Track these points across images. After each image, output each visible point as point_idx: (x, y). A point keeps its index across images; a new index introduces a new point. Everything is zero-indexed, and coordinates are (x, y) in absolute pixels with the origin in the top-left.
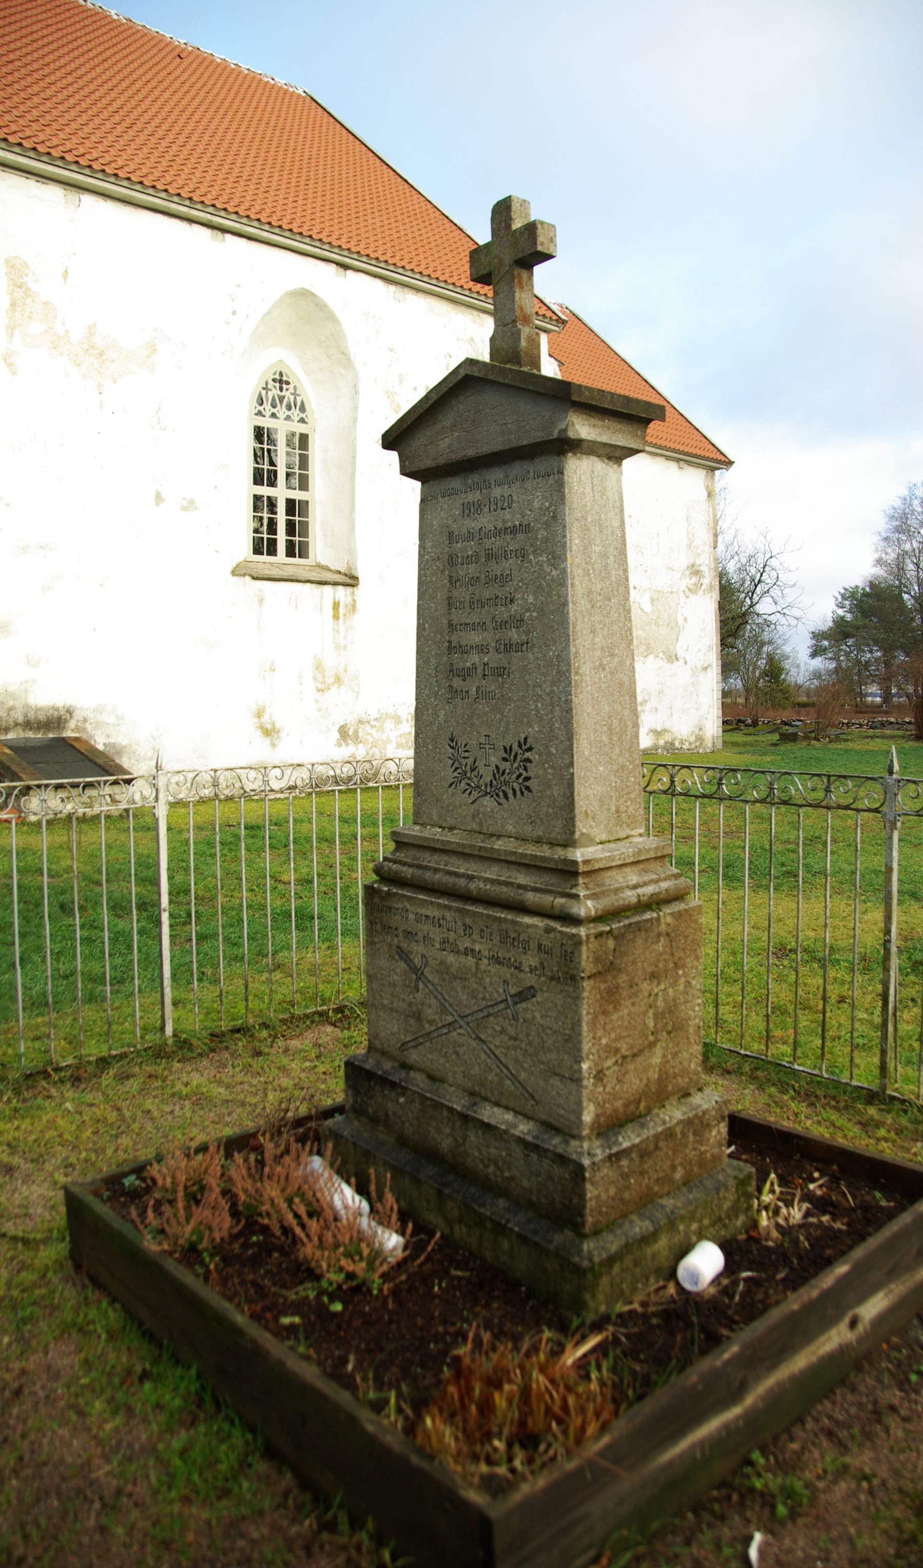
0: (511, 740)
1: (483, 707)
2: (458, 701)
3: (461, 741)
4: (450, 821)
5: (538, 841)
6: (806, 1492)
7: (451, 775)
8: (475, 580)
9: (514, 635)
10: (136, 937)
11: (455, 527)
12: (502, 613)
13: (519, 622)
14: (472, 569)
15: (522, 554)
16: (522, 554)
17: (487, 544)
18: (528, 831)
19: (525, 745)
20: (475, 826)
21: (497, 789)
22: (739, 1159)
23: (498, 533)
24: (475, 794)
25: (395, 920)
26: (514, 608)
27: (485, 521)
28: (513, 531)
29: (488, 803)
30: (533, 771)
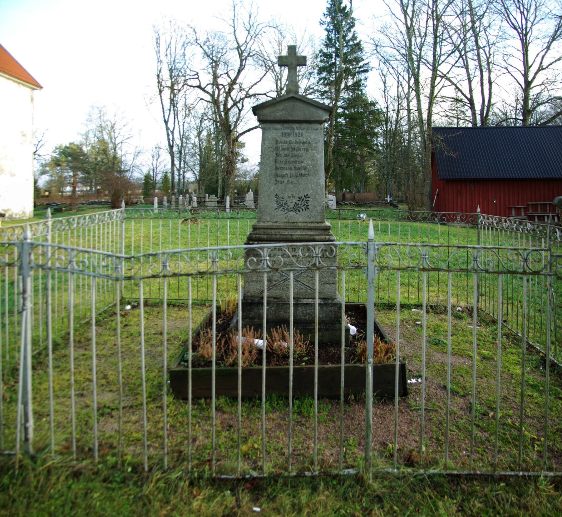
0: (301, 195)
1: (290, 186)
2: (279, 184)
3: (281, 196)
4: (275, 220)
5: (312, 222)
6: (136, 313)
7: (276, 206)
8: (286, 156)
9: (303, 172)
10: (72, 309)
11: (279, 139)
12: (298, 165)
13: (305, 168)
14: (286, 152)
15: (307, 150)
16: (307, 150)
17: (293, 145)
18: (308, 220)
19: (307, 196)
20: (286, 220)
21: (296, 209)
22: (415, 219)
23: (296, 143)
24: (286, 211)
25: (412, 402)
26: (303, 165)
27: (292, 138)
28: (303, 143)
29: (292, 213)
30: (309, 203)
